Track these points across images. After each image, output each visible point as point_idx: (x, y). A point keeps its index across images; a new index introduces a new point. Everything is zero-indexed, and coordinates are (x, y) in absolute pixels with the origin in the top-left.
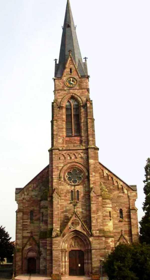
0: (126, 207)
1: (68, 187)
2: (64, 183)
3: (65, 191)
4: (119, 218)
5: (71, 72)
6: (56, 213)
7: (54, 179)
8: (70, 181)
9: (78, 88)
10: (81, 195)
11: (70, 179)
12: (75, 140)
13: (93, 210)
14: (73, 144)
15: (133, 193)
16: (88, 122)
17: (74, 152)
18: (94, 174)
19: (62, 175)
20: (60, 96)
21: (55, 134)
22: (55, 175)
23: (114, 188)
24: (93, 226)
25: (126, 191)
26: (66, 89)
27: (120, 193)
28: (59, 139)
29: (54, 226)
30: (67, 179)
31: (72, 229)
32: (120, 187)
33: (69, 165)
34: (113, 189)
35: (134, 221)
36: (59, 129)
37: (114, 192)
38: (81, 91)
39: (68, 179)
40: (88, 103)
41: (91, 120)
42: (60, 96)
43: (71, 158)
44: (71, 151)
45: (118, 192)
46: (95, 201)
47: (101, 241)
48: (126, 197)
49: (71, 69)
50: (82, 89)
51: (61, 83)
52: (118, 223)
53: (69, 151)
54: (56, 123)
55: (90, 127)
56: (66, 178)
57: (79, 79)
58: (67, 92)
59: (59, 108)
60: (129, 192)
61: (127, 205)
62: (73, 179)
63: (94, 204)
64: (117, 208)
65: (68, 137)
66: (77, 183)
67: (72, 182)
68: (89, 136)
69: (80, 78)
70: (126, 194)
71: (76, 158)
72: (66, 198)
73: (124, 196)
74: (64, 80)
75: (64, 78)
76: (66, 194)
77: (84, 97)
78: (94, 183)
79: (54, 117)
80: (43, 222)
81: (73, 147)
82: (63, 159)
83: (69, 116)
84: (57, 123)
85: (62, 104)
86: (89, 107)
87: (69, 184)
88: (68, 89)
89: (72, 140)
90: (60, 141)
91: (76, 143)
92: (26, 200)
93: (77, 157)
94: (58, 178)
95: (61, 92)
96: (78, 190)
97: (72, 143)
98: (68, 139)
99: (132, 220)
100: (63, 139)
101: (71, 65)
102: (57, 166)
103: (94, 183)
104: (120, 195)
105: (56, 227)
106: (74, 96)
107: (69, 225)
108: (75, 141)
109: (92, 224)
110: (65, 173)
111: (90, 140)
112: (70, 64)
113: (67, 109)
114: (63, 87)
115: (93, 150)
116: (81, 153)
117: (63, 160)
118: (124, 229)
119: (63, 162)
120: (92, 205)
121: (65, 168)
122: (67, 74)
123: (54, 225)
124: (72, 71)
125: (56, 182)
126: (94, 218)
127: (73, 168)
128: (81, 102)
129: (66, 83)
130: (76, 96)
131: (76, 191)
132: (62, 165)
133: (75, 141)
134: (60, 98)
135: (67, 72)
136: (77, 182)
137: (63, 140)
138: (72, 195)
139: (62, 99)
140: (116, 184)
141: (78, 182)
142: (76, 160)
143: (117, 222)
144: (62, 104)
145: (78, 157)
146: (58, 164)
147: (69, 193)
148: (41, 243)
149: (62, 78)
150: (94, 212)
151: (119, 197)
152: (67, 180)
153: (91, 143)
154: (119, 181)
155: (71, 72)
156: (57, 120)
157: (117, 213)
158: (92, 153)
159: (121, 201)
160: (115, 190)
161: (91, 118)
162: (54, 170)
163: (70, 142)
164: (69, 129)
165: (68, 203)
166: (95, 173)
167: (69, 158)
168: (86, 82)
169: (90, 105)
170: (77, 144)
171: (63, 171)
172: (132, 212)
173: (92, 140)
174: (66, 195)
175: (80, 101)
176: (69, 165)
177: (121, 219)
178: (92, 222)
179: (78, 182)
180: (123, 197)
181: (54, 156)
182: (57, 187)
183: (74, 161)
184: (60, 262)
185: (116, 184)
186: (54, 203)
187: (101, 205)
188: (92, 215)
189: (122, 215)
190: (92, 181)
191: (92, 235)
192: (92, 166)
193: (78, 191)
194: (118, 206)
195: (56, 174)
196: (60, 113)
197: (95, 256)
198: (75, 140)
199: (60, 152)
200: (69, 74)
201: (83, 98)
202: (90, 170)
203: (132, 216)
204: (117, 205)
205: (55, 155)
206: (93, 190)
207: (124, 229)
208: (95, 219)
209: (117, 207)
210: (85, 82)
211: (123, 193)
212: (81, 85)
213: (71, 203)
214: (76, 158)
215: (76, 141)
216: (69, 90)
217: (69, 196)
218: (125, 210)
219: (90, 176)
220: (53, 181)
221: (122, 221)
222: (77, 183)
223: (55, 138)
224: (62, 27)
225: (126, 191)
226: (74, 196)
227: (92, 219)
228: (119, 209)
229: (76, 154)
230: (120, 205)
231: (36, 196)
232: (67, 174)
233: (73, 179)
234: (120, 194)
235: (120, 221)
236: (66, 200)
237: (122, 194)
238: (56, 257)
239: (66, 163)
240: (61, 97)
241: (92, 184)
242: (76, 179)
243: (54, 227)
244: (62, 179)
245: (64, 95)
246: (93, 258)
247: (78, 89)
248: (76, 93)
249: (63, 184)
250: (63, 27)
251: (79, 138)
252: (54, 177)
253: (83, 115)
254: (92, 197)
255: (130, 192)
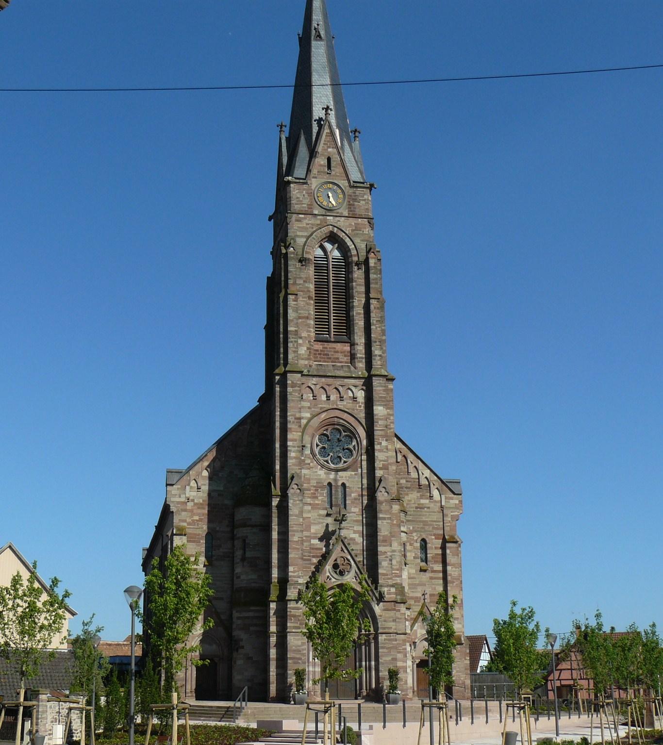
0: (434, 535)
1: (322, 473)
2: (312, 462)
3: (313, 483)
4: (419, 560)
5: (329, 167)
6: (296, 539)
7: (291, 451)
8: (326, 459)
9: (346, 213)
10: (351, 495)
11: (324, 452)
12: (337, 352)
13: (384, 536)
14: (332, 362)
15: (452, 499)
16: (372, 307)
17: (338, 382)
18: (384, 443)
19: (307, 439)
20: (302, 229)
21: (291, 331)
22: (292, 440)
23: (409, 485)
24: (384, 574)
25: (435, 493)
26: (316, 212)
27: (423, 497)
28: (301, 345)
29: (291, 572)
30: (317, 450)
31: (333, 580)
32: (424, 482)
33: (323, 416)
34: (406, 488)
35: (455, 571)
36: (300, 318)
37: (407, 494)
38: (353, 221)
39: (319, 453)
40: (372, 258)
41: (378, 302)
42: (302, 229)
43: (328, 397)
44: (330, 380)
45: (419, 495)
46: (386, 512)
47: (398, 615)
48: (437, 508)
49: (329, 160)
50: (355, 217)
51: (306, 196)
52: (415, 576)
53: (323, 380)
54: (294, 301)
55: (375, 322)
56: (316, 450)
57: (348, 188)
58: (319, 222)
59: (300, 261)
60: (443, 497)
61: (437, 529)
62: (331, 454)
63: (384, 519)
64: (415, 536)
65: (320, 343)
66: (341, 465)
67: (330, 462)
68: (373, 344)
69: (351, 187)
70: (436, 502)
71: (341, 398)
72: (317, 502)
73: (432, 505)
74: (313, 187)
75: (313, 182)
76: (317, 490)
77: (362, 241)
78: (385, 468)
79: (290, 286)
80: (245, 564)
81: (331, 368)
82: (310, 400)
83: (321, 287)
84: (297, 301)
85: (307, 253)
86: (374, 267)
87: (323, 466)
88: (323, 212)
89: (330, 351)
90: (303, 350)
91: (338, 358)
92: (195, 504)
93: (343, 397)
94: (298, 447)
95: (305, 218)
96: (345, 482)
97: (330, 358)
98: (319, 346)
99: (449, 568)
100: (308, 346)
101: (329, 147)
102: (298, 415)
103: (385, 468)
104: (423, 504)
105: (296, 574)
106: (336, 234)
107: (327, 570)
108: (336, 355)
109: (380, 571)
110: (313, 437)
111: (376, 355)
112: (327, 144)
113: (318, 267)
114: (310, 206)
115: (382, 381)
116: (353, 389)
117: (309, 401)
118: (429, 591)
119: (309, 408)
120: (379, 522)
121: (316, 422)
122: (318, 172)
123: (291, 569)
124: (333, 164)
125: (295, 458)
126: (384, 556)
127: (334, 424)
128: (354, 252)
129: (318, 197)
130: (342, 235)
131: (340, 483)
132: (308, 415)
133: (336, 355)
134: (302, 236)
135: (321, 165)
136: (326, 459)
137: (308, 349)
138: (330, 495)
139: (308, 238)
140: (414, 475)
141: (345, 462)
142: (341, 405)
143: (413, 571)
144: (307, 253)
145: (345, 397)
146: (300, 412)
147: (323, 487)
148: (238, 618)
149: (309, 182)
150: (385, 541)
151: (420, 507)
152: (317, 454)
153: (379, 363)
154: (421, 466)
155: (329, 167)
156: (297, 294)
157: (414, 548)
158: (381, 388)
159: (424, 519)
160: (412, 490)
161: (379, 299)
162: (289, 426)
163: (324, 355)
164: (322, 323)
165: (320, 515)
166: (386, 440)
167: (324, 398)
168: (365, 200)
169: (375, 263)
170: (341, 362)
171: (310, 430)
172: (450, 548)
173: (380, 356)
174: (315, 494)
175: (350, 250)
176: (323, 416)
177: (423, 564)
178: (381, 564)
179: (345, 462)
180: (429, 508)
181: (289, 389)
182: (298, 471)
183: (335, 407)
184: (304, 663)
185: (414, 475)
186: (290, 512)
187: (398, 523)
188: (380, 549)
189: (426, 554)
190: (381, 461)
191: (381, 599)
192: (380, 422)
193: (343, 485)
194: (416, 531)
195: (295, 437)
196: (303, 275)
197: (385, 650)
198: (337, 352)
199: (304, 379)
200: (324, 172)
201: (357, 240)
202: (376, 433)
203: (450, 558)
204: (413, 528)
205: (292, 387)
206: (382, 484)
207: (429, 591)
208: (387, 557)
209: (414, 534)
210: (363, 200)
211: (431, 497)
212: (354, 205)
213: (328, 515)
214: (341, 398)
215: (340, 356)
216: (325, 217)
217: (322, 497)
218: (434, 545)
219: (377, 447)
220: (289, 455)
221: (425, 571)
222: (341, 465)
223: (292, 342)
224: (299, 35)
225: (435, 493)
226: (336, 496)
227: (380, 558)
228: (420, 539)
229: (341, 389)
230: (423, 530)
231: (219, 495)
232: (319, 439)
233: (331, 454)
234: (423, 501)
235: (423, 570)
236: (314, 507)
237: (427, 501)
238: (294, 651)
239: (318, 410)
240: (306, 234)
241: (381, 469)
242: (340, 455)
243: (290, 574)
244: (307, 452)
245: (313, 228)
246: (382, 656)
247: (347, 217)
248: (343, 227)
249: (309, 464)
250: (300, 36)
251: (347, 348)
252: (289, 443)
253: (359, 288)
254: (381, 503)
255: (446, 498)
